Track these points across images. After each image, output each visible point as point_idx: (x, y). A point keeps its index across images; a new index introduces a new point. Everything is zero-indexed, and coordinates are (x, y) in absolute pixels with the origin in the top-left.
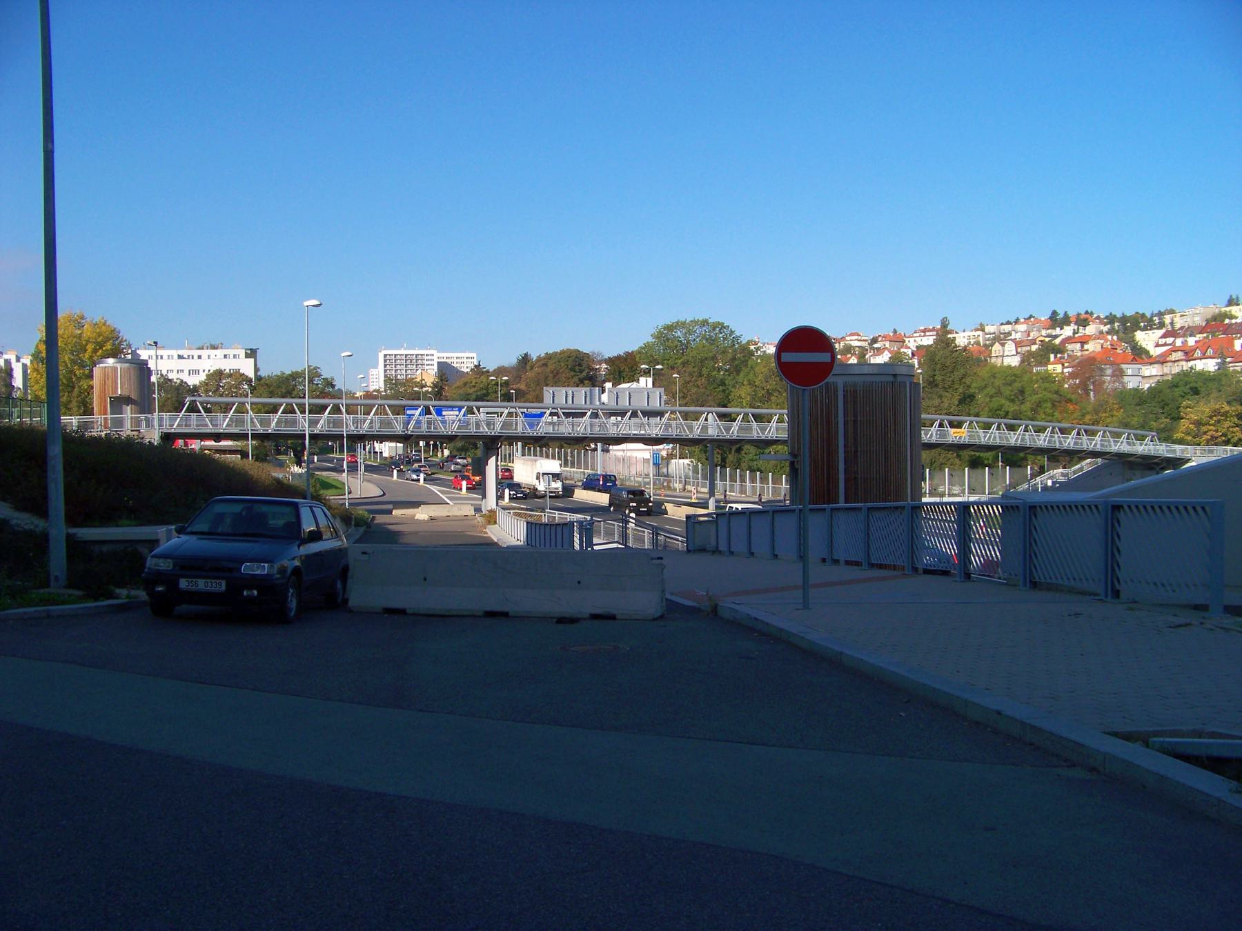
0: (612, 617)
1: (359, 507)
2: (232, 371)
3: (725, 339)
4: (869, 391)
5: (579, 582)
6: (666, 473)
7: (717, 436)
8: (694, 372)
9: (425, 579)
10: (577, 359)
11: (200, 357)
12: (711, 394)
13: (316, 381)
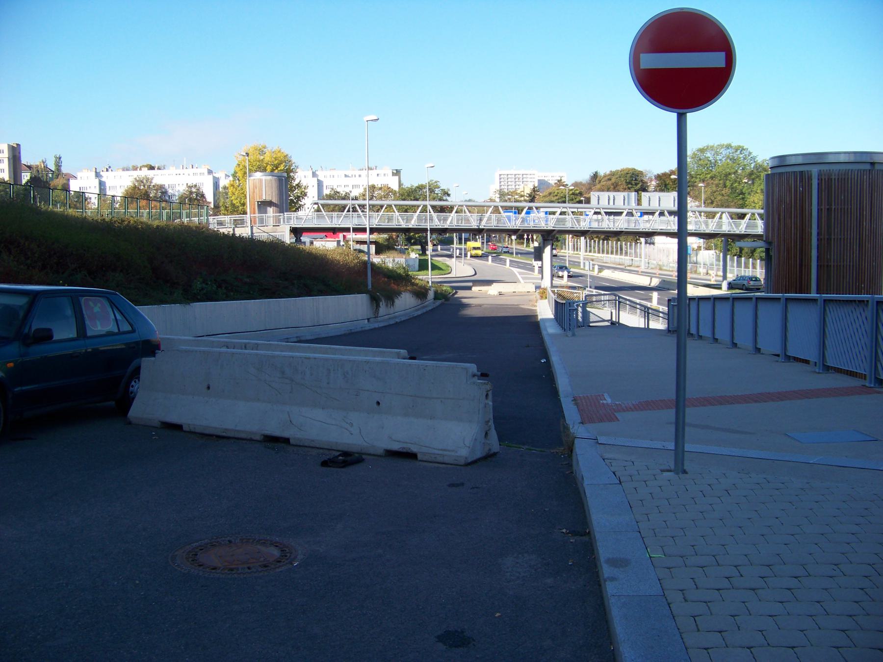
0: (412, 456)
1: (445, 284)
2: (383, 186)
3: (745, 159)
4: (845, 179)
5: (378, 403)
6: (695, 261)
7: (729, 231)
8: (720, 184)
9: (209, 388)
10: (633, 176)
11: (360, 176)
12: (733, 201)
13: (437, 191)
